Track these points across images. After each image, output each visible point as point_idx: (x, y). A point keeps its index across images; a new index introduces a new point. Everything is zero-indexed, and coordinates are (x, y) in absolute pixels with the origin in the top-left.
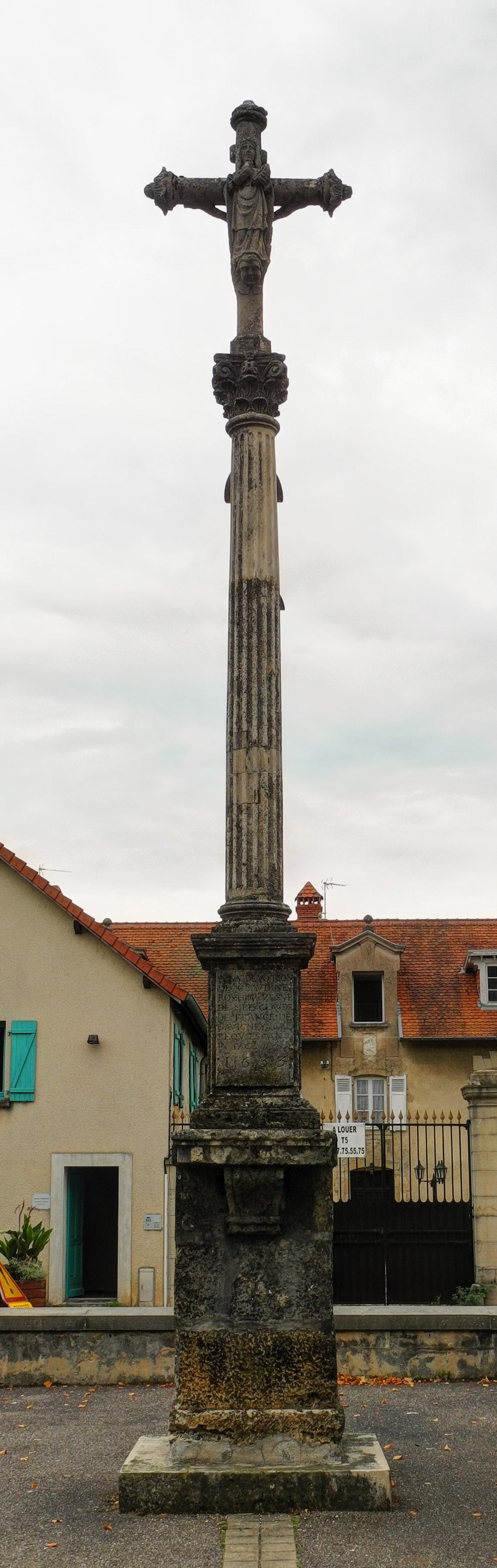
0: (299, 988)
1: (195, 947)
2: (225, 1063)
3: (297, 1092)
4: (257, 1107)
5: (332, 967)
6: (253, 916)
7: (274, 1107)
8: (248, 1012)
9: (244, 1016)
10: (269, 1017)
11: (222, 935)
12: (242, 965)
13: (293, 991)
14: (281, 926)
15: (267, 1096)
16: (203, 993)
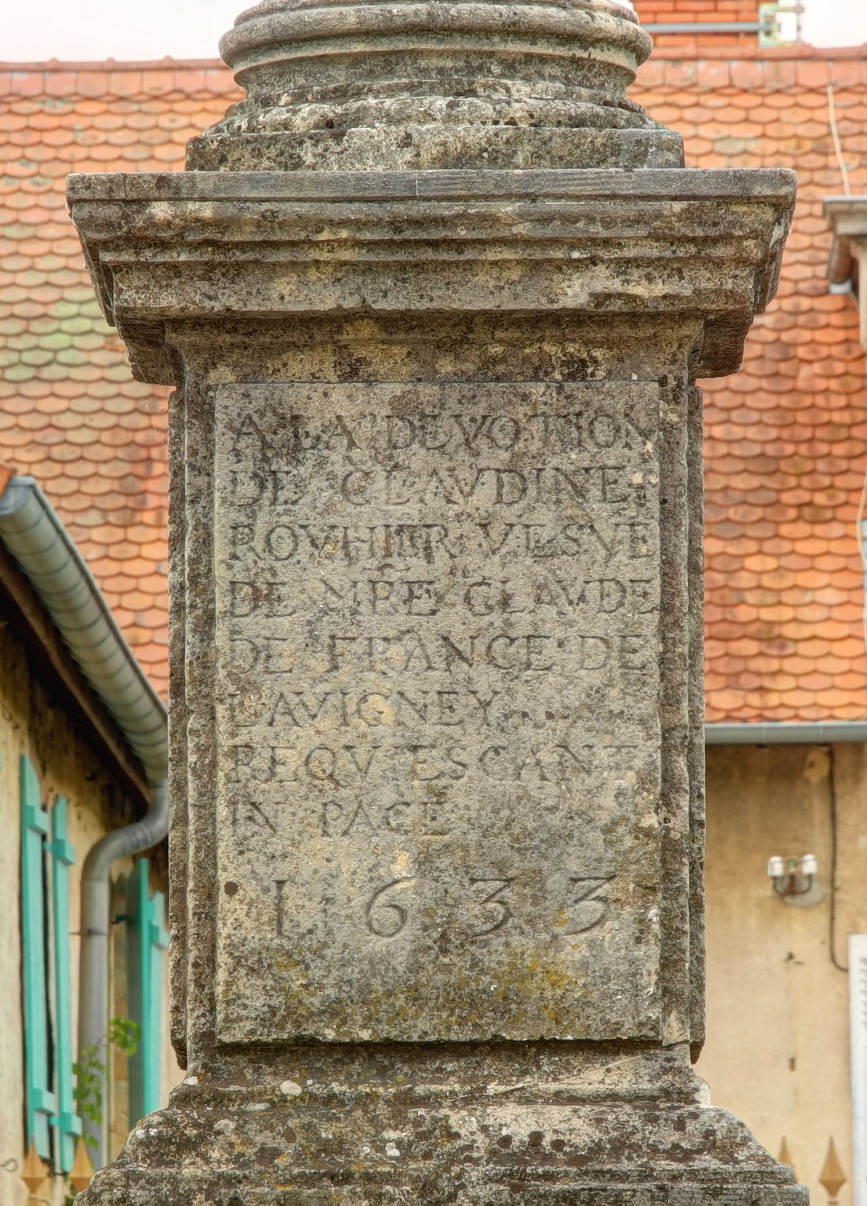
0: (694, 489)
1: (92, 249)
2: (269, 912)
3: (679, 1071)
4: (453, 1159)
5: (835, 320)
6: (425, 71)
7: (547, 1158)
8: (401, 620)
9: (380, 646)
10: (519, 650)
11: (254, 182)
12: (361, 353)
13: (654, 505)
14: (590, 131)
15: (505, 1094)
16: (88, 469)
